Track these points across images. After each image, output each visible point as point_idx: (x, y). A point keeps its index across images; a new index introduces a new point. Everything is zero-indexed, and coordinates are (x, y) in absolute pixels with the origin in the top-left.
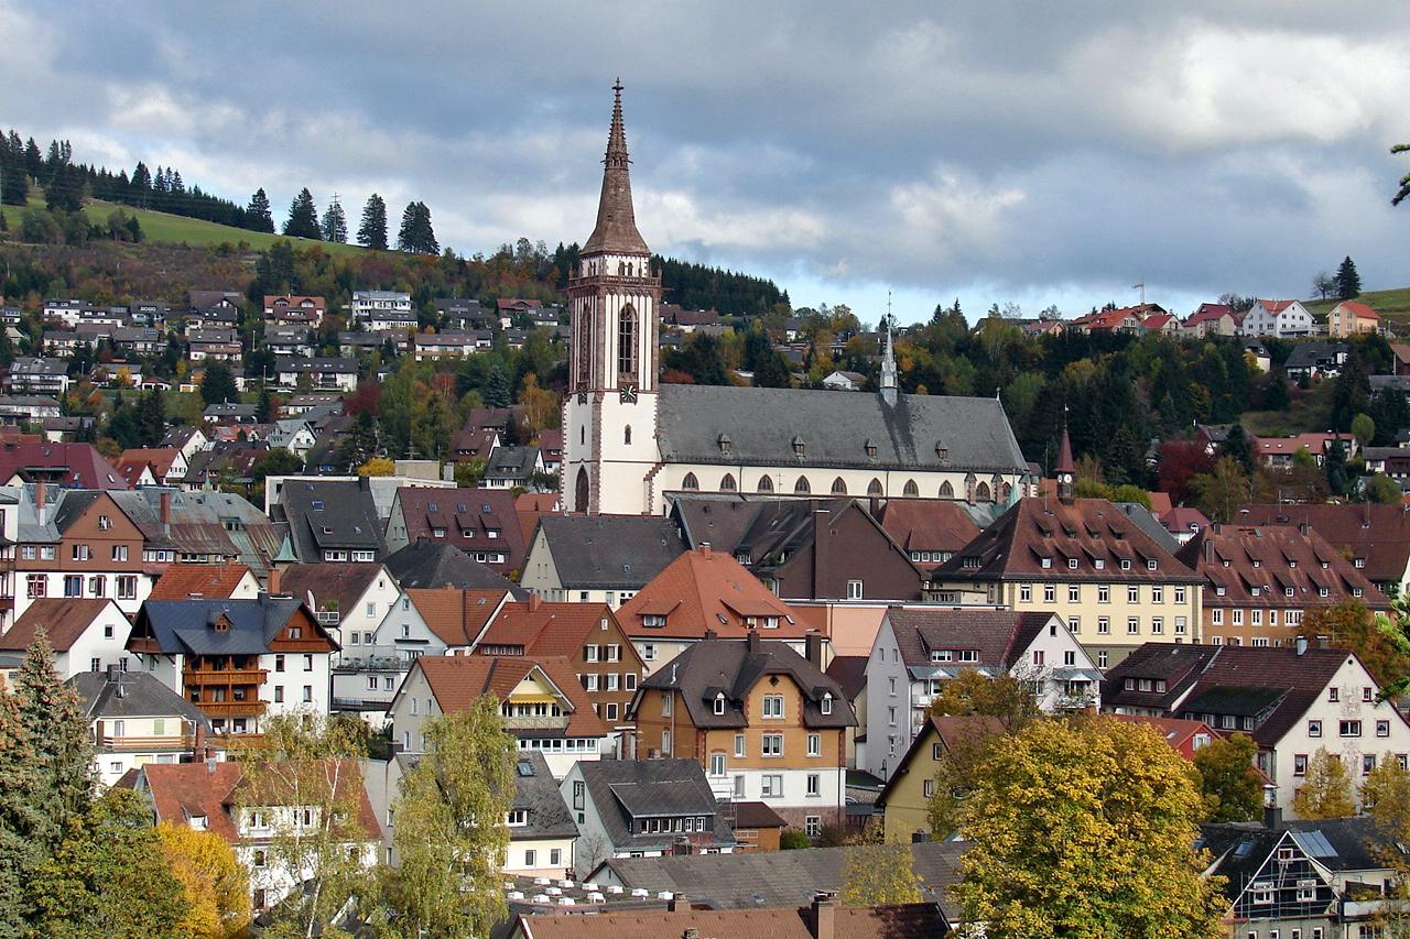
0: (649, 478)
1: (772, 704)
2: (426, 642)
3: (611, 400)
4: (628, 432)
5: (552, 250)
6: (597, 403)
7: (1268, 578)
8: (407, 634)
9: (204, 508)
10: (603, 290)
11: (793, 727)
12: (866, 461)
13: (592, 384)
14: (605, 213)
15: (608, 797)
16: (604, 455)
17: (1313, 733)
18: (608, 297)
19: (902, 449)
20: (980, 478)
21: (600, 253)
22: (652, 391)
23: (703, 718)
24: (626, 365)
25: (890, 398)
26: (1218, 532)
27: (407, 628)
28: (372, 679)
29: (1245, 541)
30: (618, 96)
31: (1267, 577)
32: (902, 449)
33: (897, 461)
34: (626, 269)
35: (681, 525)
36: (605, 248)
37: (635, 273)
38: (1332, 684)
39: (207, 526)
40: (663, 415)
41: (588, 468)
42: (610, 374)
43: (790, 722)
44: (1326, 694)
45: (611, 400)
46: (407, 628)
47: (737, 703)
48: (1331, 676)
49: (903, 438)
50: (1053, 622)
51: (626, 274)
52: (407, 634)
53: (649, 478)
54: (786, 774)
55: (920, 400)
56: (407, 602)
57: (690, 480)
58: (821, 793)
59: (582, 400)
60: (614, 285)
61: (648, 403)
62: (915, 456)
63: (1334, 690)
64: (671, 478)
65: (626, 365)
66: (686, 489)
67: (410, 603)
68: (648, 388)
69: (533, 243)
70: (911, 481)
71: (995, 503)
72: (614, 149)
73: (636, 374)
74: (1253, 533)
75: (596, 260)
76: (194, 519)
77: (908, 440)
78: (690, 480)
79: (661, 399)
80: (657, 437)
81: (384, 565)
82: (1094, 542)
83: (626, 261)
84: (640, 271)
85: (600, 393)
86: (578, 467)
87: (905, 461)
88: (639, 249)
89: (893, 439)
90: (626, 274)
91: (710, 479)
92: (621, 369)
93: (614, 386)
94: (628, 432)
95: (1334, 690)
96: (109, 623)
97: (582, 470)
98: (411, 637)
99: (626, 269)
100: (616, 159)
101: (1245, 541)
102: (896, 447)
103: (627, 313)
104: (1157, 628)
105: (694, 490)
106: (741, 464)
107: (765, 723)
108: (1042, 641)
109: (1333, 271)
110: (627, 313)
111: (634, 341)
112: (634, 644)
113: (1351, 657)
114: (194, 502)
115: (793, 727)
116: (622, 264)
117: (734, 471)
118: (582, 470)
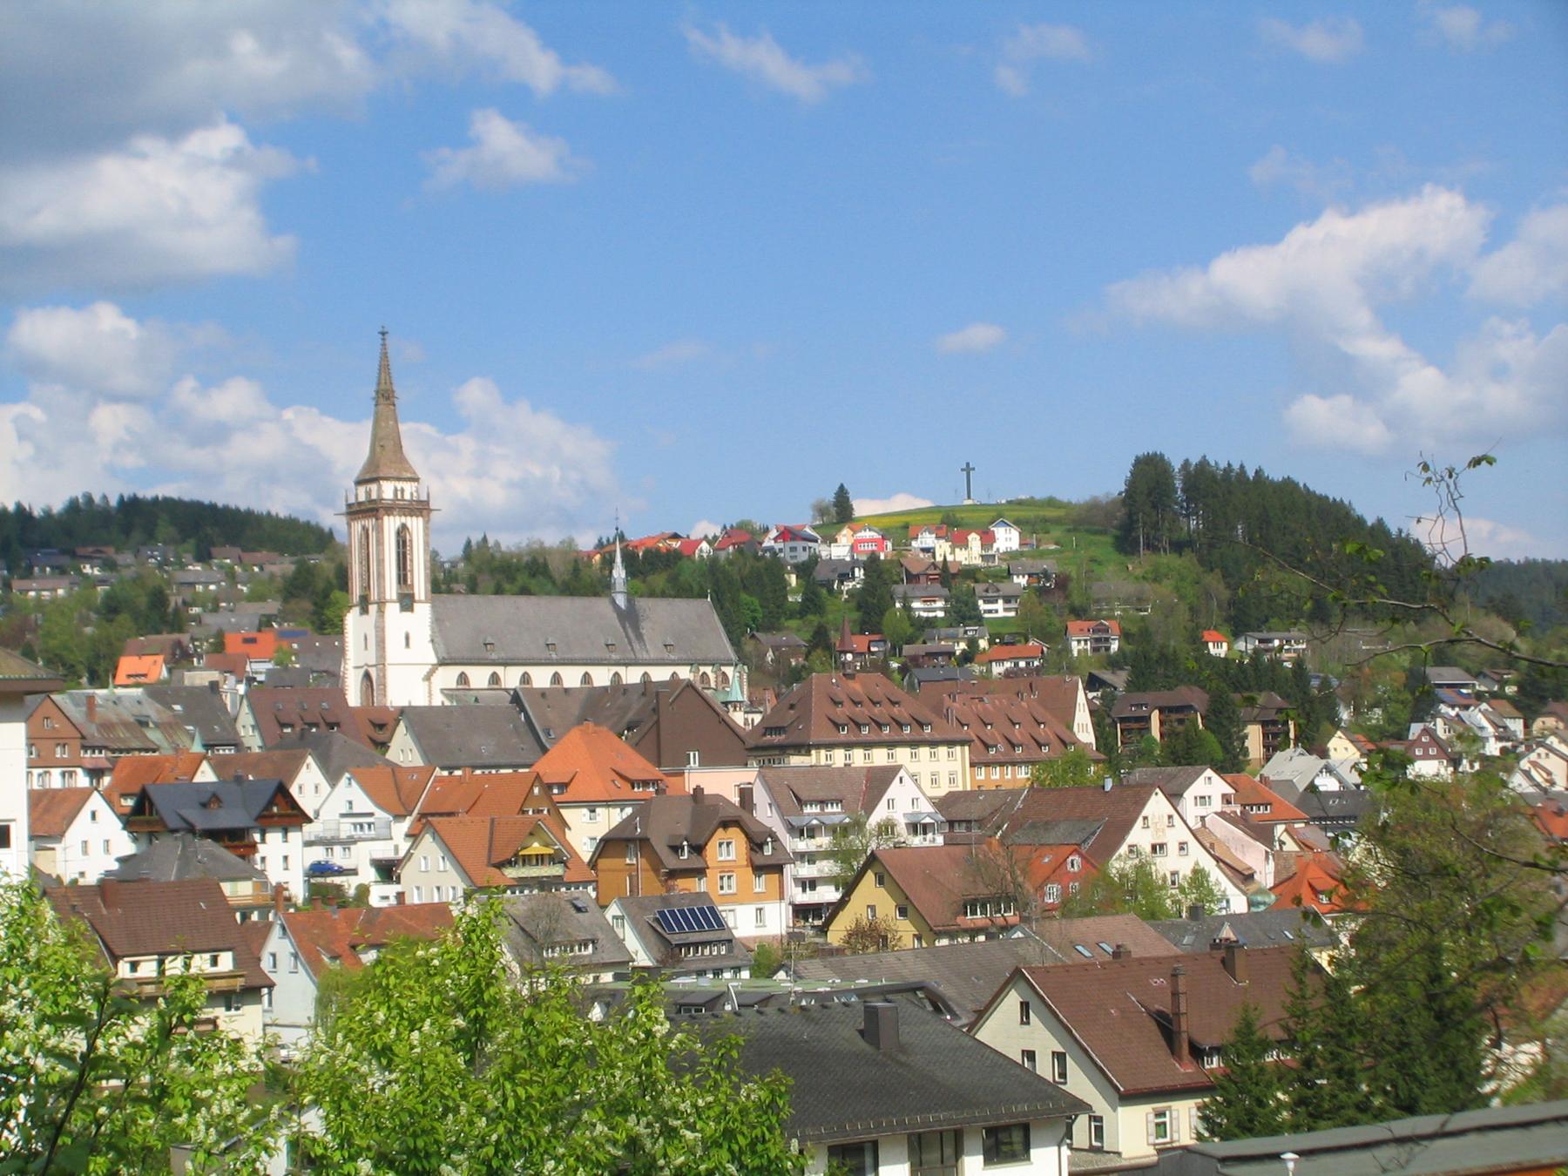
0: (428, 678)
1: (724, 846)
2: (371, 815)
3: (393, 609)
4: (407, 638)
5: (113, 502)
6: (381, 612)
7: (999, 738)
8: (351, 808)
9: (120, 709)
10: (382, 511)
11: (741, 867)
12: (608, 656)
13: (374, 596)
14: (377, 441)
15: (646, 929)
16: (388, 660)
17: (1182, 852)
18: (386, 518)
19: (637, 646)
20: (703, 669)
21: (375, 480)
22: (426, 602)
23: (671, 862)
24: (403, 577)
25: (621, 600)
26: (954, 700)
27: (350, 803)
28: (327, 849)
29: (977, 708)
30: (384, 339)
31: (999, 738)
32: (637, 646)
33: (633, 657)
34: (399, 493)
35: (523, 709)
36: (381, 475)
37: (407, 497)
38: (1144, 813)
39: (126, 725)
40: (438, 620)
41: (373, 672)
42: (392, 589)
43: (738, 863)
44: (1140, 821)
45: (393, 609)
46: (350, 803)
47: (698, 849)
48: (1143, 805)
49: (636, 636)
50: (902, 773)
51: (399, 497)
52: (351, 808)
53: (428, 678)
54: (739, 908)
55: (643, 604)
56: (349, 779)
57: (463, 678)
58: (767, 923)
59: (365, 611)
60: (390, 509)
61: (423, 611)
62: (647, 652)
63: (1145, 818)
64: (448, 677)
65: (403, 577)
66: (460, 687)
67: (353, 782)
68: (423, 598)
69: (97, 499)
70: (674, 673)
71: (715, 690)
72: (383, 387)
73: (412, 586)
74: (981, 700)
75: (374, 487)
76: (114, 719)
77: (640, 637)
78: (463, 678)
79: (433, 607)
80: (432, 641)
81: (310, 750)
82: (877, 710)
83: (399, 485)
84: (412, 494)
85: (381, 604)
86: (362, 672)
87: (639, 656)
88: (409, 475)
89: (627, 636)
90: (399, 497)
91: (479, 677)
92: (399, 582)
93: (394, 597)
94: (407, 638)
95: (1145, 818)
96: (93, 809)
97: (367, 676)
98: (355, 810)
99: (399, 493)
100: (385, 396)
101: (977, 708)
102: (630, 643)
103: (402, 532)
104: (952, 781)
105: (496, 687)
106: (505, 664)
107: (720, 864)
108: (894, 790)
109: (830, 496)
110: (402, 532)
111: (408, 557)
112: (561, 811)
113: (1158, 790)
114: (111, 704)
115: (741, 867)
116: (396, 490)
117: (500, 670)
118: (367, 676)
